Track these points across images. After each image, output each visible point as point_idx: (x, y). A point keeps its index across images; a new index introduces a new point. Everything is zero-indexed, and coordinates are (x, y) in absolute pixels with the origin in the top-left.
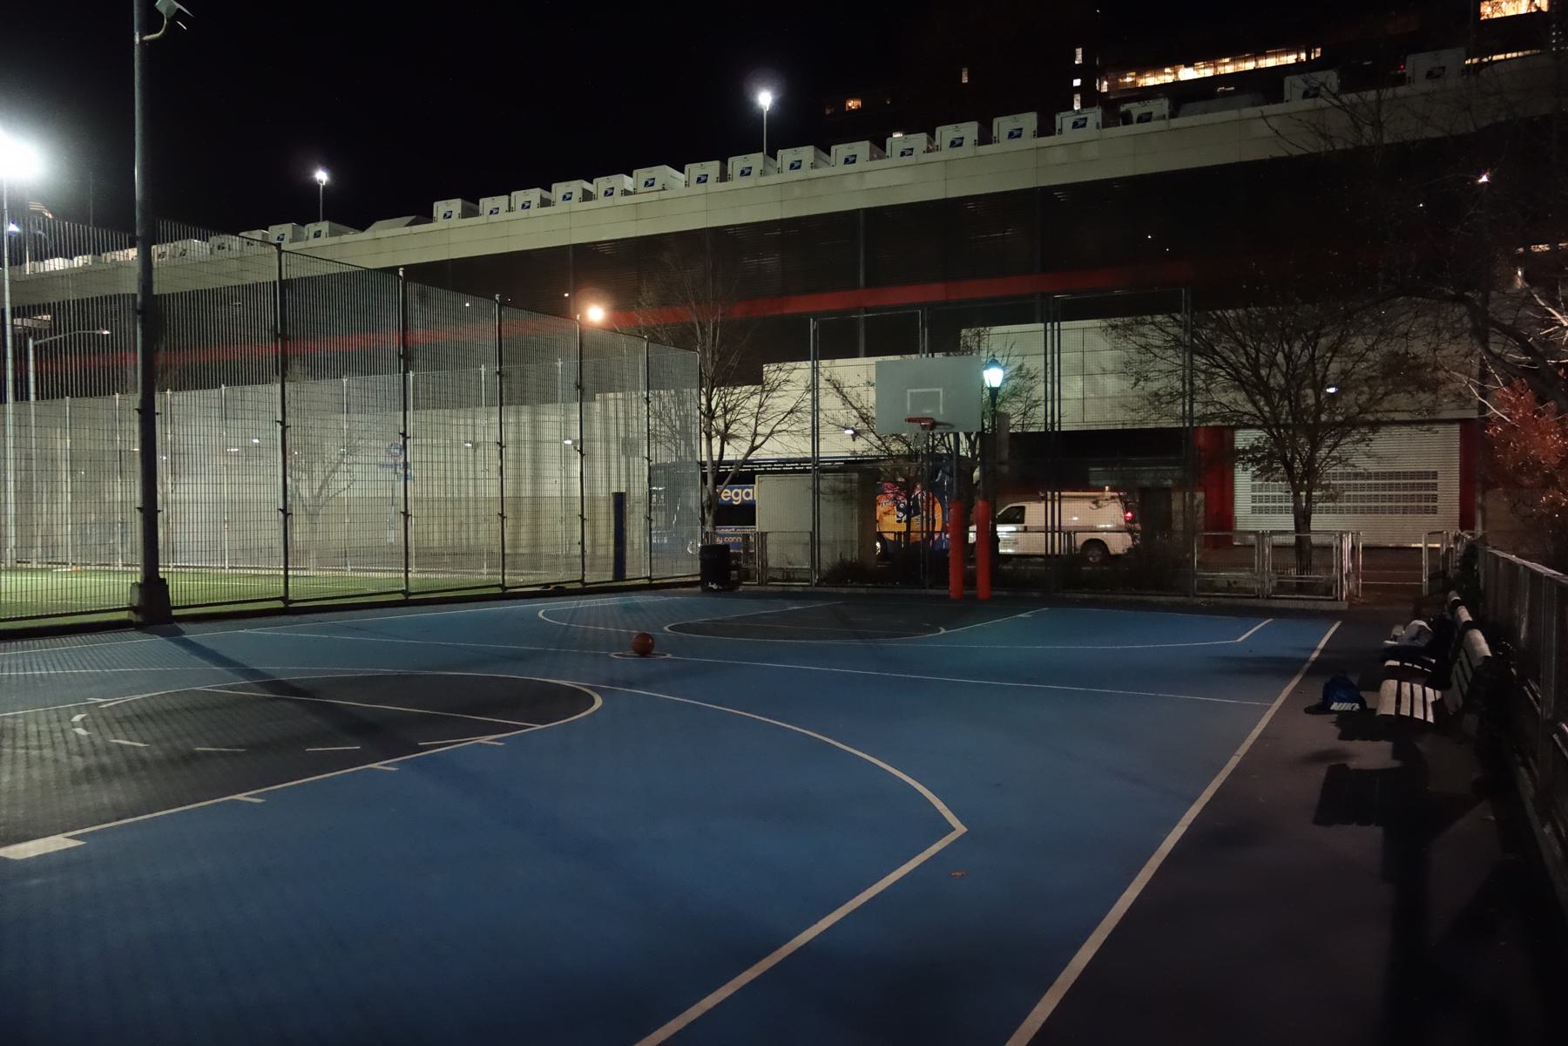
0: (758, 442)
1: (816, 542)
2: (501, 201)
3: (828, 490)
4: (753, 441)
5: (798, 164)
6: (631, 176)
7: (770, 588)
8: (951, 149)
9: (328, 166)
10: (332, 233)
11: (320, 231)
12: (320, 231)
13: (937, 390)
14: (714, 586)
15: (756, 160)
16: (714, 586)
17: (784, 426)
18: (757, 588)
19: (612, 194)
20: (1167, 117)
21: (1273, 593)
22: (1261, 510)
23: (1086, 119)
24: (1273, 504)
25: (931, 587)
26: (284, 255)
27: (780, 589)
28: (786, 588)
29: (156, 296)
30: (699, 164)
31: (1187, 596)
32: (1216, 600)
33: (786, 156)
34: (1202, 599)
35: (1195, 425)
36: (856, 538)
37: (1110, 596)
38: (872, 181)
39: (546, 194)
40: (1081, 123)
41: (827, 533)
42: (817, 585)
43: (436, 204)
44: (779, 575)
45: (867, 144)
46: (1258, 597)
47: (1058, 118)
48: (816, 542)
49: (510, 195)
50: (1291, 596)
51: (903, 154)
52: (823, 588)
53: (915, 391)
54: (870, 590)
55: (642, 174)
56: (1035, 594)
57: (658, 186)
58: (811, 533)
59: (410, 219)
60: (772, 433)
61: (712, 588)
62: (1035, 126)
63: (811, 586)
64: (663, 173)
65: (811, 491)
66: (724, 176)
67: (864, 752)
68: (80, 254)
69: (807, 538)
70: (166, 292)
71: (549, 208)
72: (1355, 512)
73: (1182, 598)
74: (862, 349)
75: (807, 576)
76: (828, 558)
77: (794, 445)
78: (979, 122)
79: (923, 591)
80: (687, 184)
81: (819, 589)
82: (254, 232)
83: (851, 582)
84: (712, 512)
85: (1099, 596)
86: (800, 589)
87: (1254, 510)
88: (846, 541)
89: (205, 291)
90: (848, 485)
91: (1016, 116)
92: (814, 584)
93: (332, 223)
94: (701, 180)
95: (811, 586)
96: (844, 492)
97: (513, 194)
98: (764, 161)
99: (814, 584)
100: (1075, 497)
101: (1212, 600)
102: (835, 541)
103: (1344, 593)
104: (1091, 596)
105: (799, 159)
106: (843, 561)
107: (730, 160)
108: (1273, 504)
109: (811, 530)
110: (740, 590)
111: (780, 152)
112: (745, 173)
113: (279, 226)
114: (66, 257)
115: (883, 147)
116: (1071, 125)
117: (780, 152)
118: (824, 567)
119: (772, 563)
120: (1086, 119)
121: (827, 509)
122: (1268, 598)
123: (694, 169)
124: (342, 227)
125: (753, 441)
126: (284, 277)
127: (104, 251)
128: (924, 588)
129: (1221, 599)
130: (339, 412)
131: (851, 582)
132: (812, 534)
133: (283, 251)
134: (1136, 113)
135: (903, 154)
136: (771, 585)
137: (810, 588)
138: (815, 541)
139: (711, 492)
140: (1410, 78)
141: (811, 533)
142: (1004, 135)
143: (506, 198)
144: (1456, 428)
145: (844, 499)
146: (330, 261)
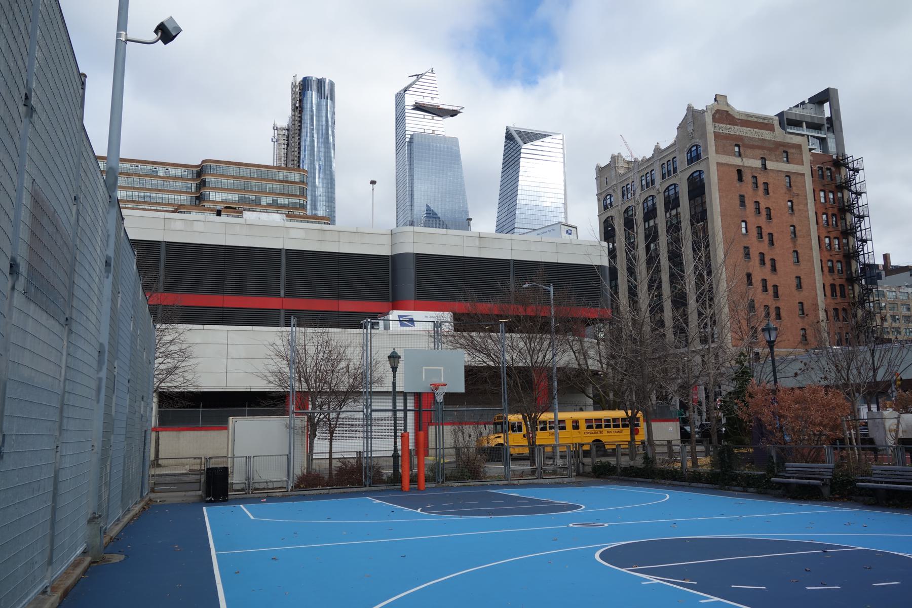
92: (289, 490)
95: (287, 491)
99: (289, 490)
109: (288, 453)
128: (365, 486)
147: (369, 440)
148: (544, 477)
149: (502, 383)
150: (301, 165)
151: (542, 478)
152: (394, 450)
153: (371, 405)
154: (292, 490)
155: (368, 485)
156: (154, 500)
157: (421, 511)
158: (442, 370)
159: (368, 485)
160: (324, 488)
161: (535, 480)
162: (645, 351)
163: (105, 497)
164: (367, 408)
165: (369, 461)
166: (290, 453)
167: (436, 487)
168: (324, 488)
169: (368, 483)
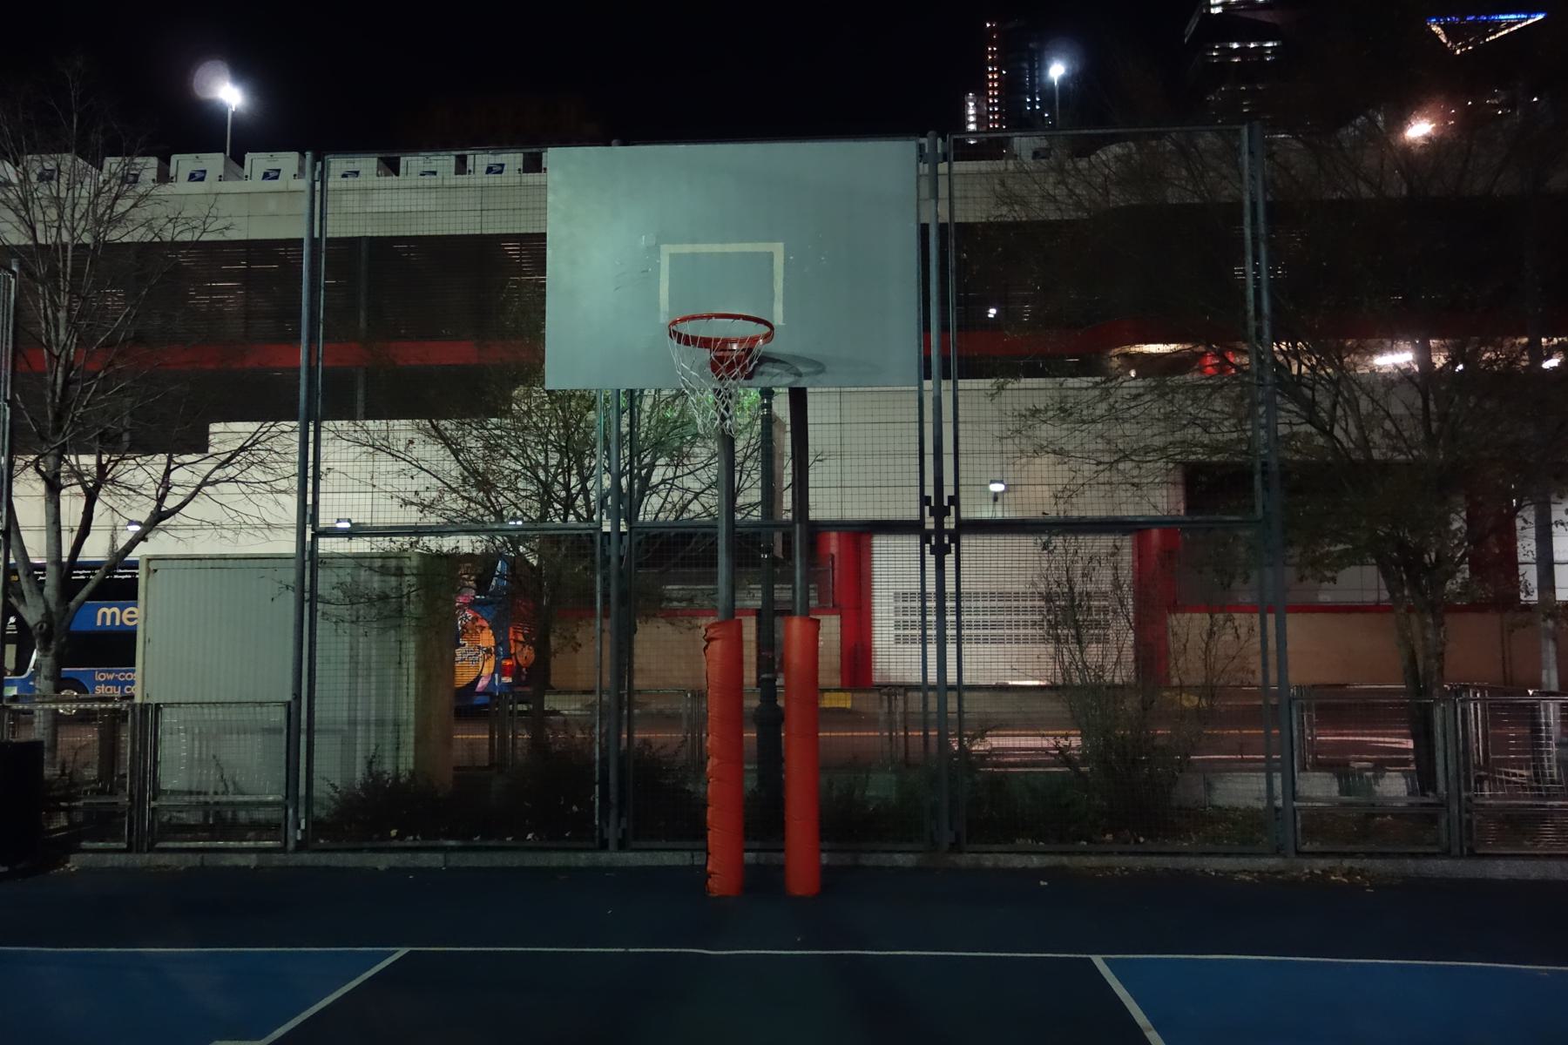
0: (170, 503)
1: (304, 726)
3: (338, 593)
4: (161, 500)
7: (164, 860)
13: (761, 247)
15: (214, 162)
17: (231, 471)
18: (120, 860)
25: (622, 846)
27: (194, 860)
28: (210, 859)
33: (257, 162)
35: (1283, 430)
36: (408, 712)
41: (332, 703)
42: (301, 847)
48: (304, 726)
53: (687, 248)
56: (902, 860)
60: (205, 483)
62: (221, 171)
65: (291, 596)
66: (164, 177)
69: (278, 716)
72: (985, 641)
74: (360, 410)
75: (274, 814)
77: (253, 510)
79: (604, 858)
81: (307, 858)
83: (400, 837)
84: (53, 645)
85: (1065, 860)
86: (252, 860)
87: (897, 639)
90: (393, 581)
91: (201, 155)
92: (291, 845)
95: (283, 850)
96: (384, 597)
98: (225, 166)
99: (291, 845)
100: (302, 637)
102: (353, 723)
106: (374, 780)
107: (174, 158)
109: (289, 697)
111: (249, 156)
112: (195, 177)
117: (249, 156)
118: (321, 789)
119: (173, 776)
121: (333, 644)
125: (161, 500)
128: (604, 846)
131: (400, 837)
132: (292, 710)
139: (53, 606)
141: (289, 703)
145: (381, 617)
147: (951, 649)
148: (1307, 847)
149: (613, 599)
150: (260, 815)
151: (1299, 853)
152: (1550, 525)
153: (954, 500)
154: (301, 847)
155: (612, 844)
156: (373, 747)
157: (481, 839)
158: (927, 145)
159: (612, 844)
160: (431, 843)
161: (276, 856)
162: (368, 723)
163: (1508, 671)
164: (940, 512)
165: (952, 705)
166: (297, 696)
167: (193, 758)
168: (431, 843)
169: (612, 833)
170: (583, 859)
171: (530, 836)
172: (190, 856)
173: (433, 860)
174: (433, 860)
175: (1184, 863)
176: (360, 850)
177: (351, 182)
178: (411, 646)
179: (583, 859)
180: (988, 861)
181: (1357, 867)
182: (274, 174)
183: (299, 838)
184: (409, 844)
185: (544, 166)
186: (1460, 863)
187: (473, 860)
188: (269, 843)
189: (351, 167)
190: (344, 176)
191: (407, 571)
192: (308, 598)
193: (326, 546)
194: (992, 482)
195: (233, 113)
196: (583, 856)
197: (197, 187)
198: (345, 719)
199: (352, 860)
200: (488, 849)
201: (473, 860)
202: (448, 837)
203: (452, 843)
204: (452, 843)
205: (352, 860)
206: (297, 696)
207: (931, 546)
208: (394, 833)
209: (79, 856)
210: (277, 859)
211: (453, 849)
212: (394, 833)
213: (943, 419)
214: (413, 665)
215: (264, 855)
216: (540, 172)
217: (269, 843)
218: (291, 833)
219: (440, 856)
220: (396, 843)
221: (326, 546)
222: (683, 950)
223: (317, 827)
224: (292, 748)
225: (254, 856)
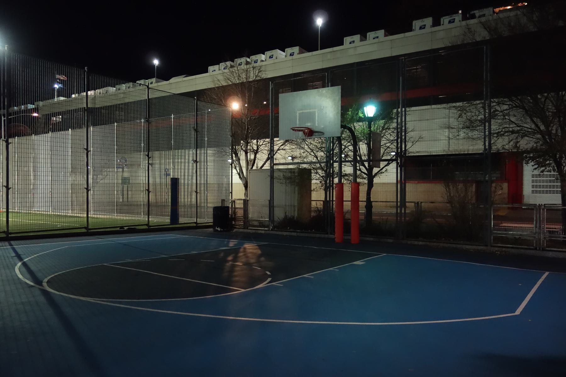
2: (216, 67)
5: (272, 56)
6: (264, 54)
8: (420, 30)
9: (311, 21)
10: (157, 82)
11: (152, 82)
12: (152, 82)
14: (219, 229)
16: (219, 229)
19: (257, 62)
20: (461, 21)
21: (547, 247)
22: (536, 192)
23: (454, 19)
24: (539, 189)
26: (150, 89)
27: (254, 231)
29: (150, 99)
30: (290, 48)
31: (486, 246)
32: (507, 250)
34: (496, 249)
36: (296, 204)
37: (435, 244)
38: (360, 50)
39: (232, 63)
40: (452, 21)
42: (272, 230)
43: (414, 22)
44: (256, 223)
45: (383, 31)
46: (536, 249)
47: (442, 20)
49: (219, 65)
50: (561, 250)
51: (350, 43)
52: (275, 232)
54: (298, 234)
55: (268, 53)
57: (274, 57)
58: (269, 200)
59: (185, 76)
61: (217, 230)
62: (298, 52)
63: (269, 230)
64: (278, 53)
67: (241, 317)
68: (98, 89)
70: (107, 105)
71: (411, 32)
73: (482, 247)
76: (279, 214)
78: (360, 35)
79: (326, 236)
80: (286, 56)
82: (141, 81)
83: (289, 229)
85: (428, 243)
86: (263, 232)
88: (291, 206)
89: (70, 110)
91: (214, 66)
92: (270, 229)
93: (301, 48)
94: (292, 55)
97: (220, 64)
99: (270, 229)
101: (504, 249)
102: (286, 205)
103: (517, 236)
104: (424, 243)
105: (293, 52)
108: (539, 189)
109: (269, 199)
110: (234, 231)
113: (270, 51)
114: (111, 87)
115: (366, 38)
116: (419, 28)
118: (276, 219)
120: (454, 19)
122: (544, 250)
123: (289, 50)
124: (159, 80)
126: (150, 97)
127: (116, 85)
128: (327, 234)
129: (509, 250)
130: (137, 151)
131: (289, 229)
132: (270, 201)
133: (150, 88)
134: (477, 15)
135: (350, 43)
136: (250, 229)
137: (268, 231)
138: (271, 206)
140: (414, 29)
141: (269, 200)
142: (418, 27)
143: (218, 66)
144: (10, 140)
146: (163, 91)
151: (492, 246)
154: (272, 230)
160: (295, 231)
170: (323, 236)
171: (313, 230)
172: (253, 230)
173: (294, 234)
174: (294, 234)
175: (459, 246)
176: (282, 231)
177: (352, 45)
178: (297, 189)
179: (323, 236)
180: (409, 242)
181: (507, 250)
182: (423, 27)
183: (272, 228)
184: (291, 231)
185: (414, 28)
186: (537, 252)
187: (302, 235)
188: (266, 229)
189: (352, 40)
190: (374, 39)
191: (295, 172)
192: (272, 177)
193: (275, 167)
194: (392, 152)
195: (320, 27)
196: (322, 235)
197: (423, 31)
198: (284, 204)
199: (280, 233)
200: (306, 233)
201: (302, 235)
202: (298, 230)
203: (299, 231)
204: (299, 231)
205: (280, 233)
206: (271, 199)
207: (399, 165)
208: (288, 228)
209: (236, 229)
210: (268, 232)
211: (299, 232)
212: (288, 228)
213: (9, 208)
214: (297, 193)
215: (266, 231)
216: (412, 31)
217: (266, 229)
218: (270, 227)
219: (296, 233)
220: (289, 230)
221: (276, 167)
222: (193, 281)
223: (274, 227)
224: (270, 211)
225: (264, 231)
